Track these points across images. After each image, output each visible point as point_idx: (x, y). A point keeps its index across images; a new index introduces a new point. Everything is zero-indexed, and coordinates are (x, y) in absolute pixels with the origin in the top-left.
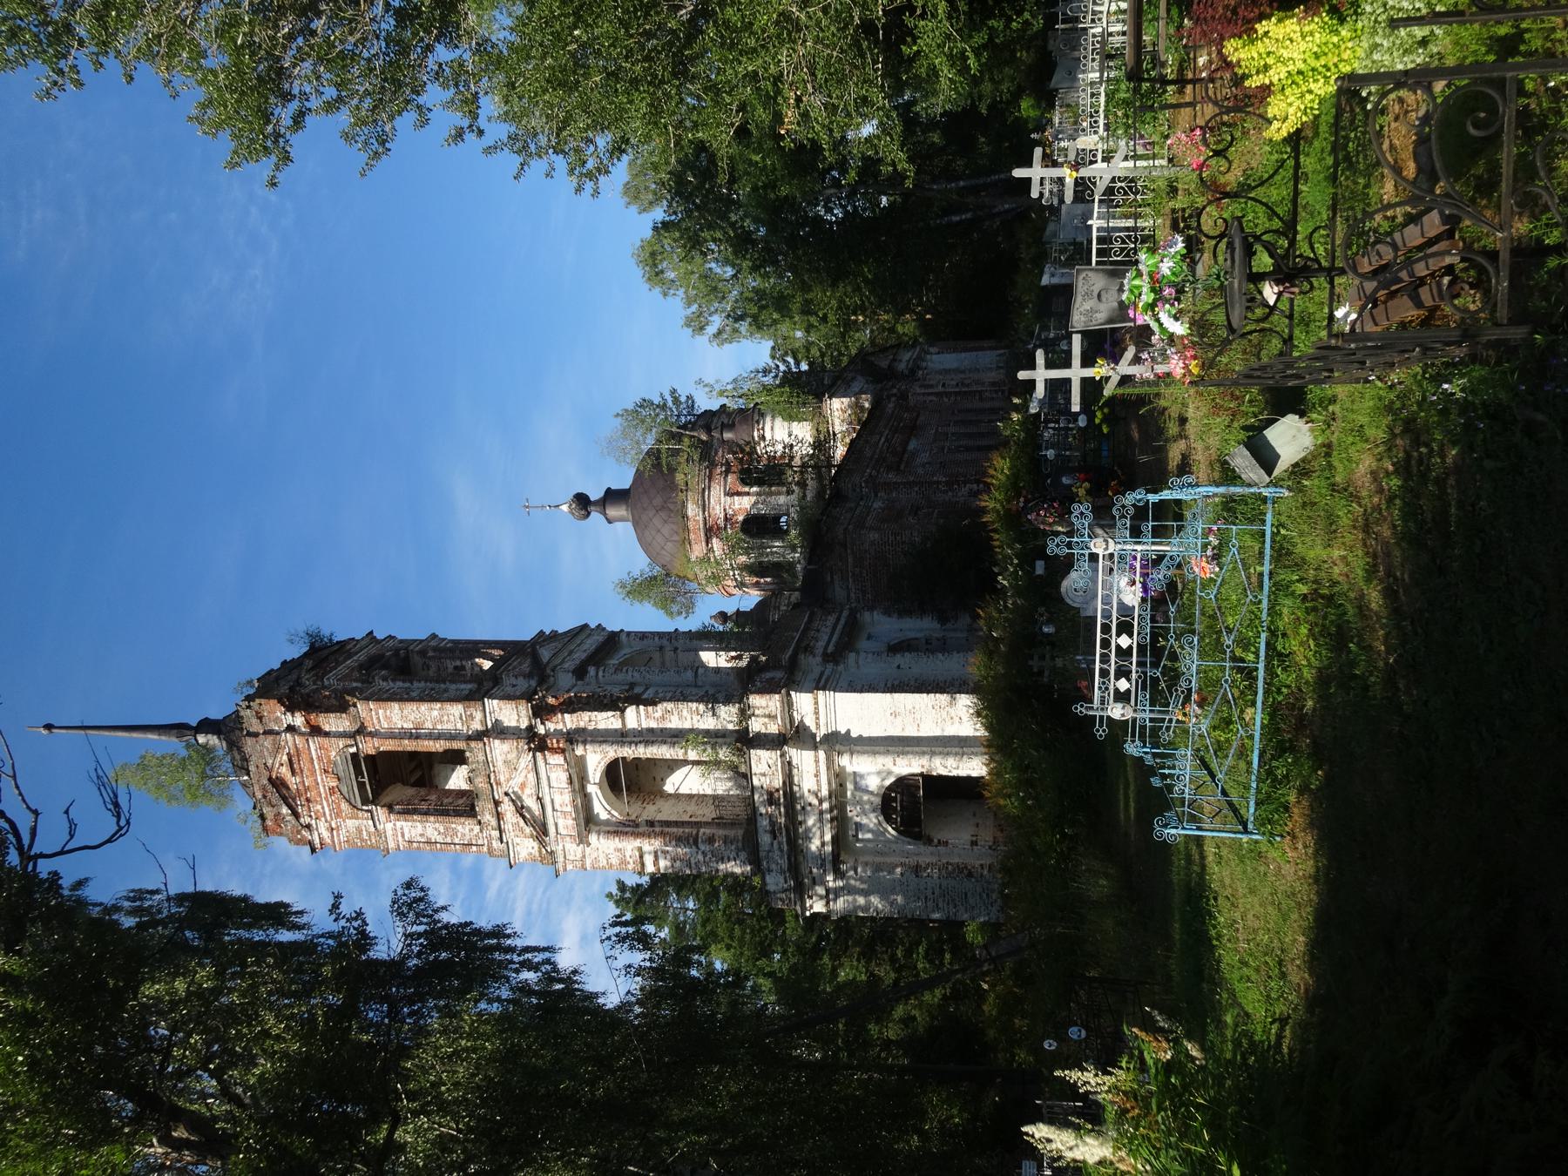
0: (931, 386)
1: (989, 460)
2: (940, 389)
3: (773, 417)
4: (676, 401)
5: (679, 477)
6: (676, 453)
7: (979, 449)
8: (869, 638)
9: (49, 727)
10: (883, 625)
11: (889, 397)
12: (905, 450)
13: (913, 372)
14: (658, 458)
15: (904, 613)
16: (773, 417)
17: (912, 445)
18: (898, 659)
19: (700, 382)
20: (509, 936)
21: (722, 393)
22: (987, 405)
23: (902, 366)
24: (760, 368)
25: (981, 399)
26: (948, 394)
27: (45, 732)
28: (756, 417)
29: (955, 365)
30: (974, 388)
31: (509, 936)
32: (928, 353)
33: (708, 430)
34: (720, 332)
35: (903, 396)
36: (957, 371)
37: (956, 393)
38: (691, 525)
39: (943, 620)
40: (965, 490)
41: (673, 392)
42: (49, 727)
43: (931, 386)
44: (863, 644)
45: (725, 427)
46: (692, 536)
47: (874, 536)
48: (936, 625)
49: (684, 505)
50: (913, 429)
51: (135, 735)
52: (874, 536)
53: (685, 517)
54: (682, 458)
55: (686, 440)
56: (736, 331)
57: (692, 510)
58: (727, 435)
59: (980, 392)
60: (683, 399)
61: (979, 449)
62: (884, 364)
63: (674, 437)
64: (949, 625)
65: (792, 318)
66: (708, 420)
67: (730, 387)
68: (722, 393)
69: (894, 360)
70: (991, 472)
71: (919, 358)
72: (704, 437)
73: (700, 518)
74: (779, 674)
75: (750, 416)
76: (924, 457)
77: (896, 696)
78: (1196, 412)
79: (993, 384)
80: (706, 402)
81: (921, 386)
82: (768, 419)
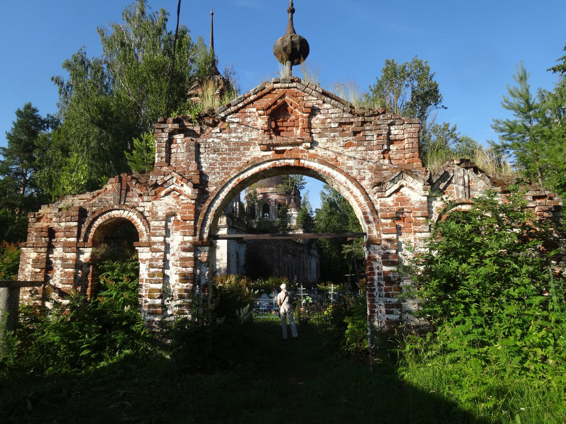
0: (306, 260)
1: (286, 277)
2: (305, 263)
3: (298, 214)
4: (303, 183)
5: (280, 185)
6: (288, 185)
7: (288, 275)
8: (239, 247)
9: (212, 14)
10: (243, 250)
11: (303, 248)
12: (288, 254)
13: (310, 254)
14: (286, 179)
15: (245, 255)
16: (298, 214)
17: (290, 256)
18: (235, 255)
19: (308, 191)
20: (285, 311)
21: (305, 198)
22: (301, 276)
23: (312, 251)
24: (312, 210)
25: (302, 274)
26: (304, 265)
27: (211, 13)
28: (298, 209)
29: (312, 266)
30: (305, 272)
31: (285, 311)
32: (316, 258)
33: (294, 195)
34: (324, 194)
35: (303, 252)
36: (311, 267)
37: (304, 267)
38: (266, 189)
39: (244, 266)
40: (277, 271)
41: (306, 183)
42: (212, 14)
43: (306, 260)
44: (238, 245)
45: (295, 200)
46: (263, 189)
47: (266, 247)
48: (243, 264)
49: (272, 187)
50: (294, 255)
51: (211, 40)
52: (266, 247)
53: (269, 187)
54: (286, 186)
55: (292, 187)
56: (324, 199)
57: (271, 189)
58: (293, 200)
59: (304, 274)
60: (303, 186)
61: (288, 275)
62: (313, 246)
63: (293, 183)
64: (242, 267)
65: (328, 216)
66: (297, 193)
67: (307, 200)
68: (305, 198)
69: (314, 249)
70: (283, 278)
71: (314, 256)
72: (292, 193)
73: (268, 191)
74: (231, 224)
75: (298, 205)
76: (286, 259)
77: (226, 255)
78: (173, 117)
79: (306, 278)
80: (302, 193)
81: (306, 257)
82: (297, 213)
